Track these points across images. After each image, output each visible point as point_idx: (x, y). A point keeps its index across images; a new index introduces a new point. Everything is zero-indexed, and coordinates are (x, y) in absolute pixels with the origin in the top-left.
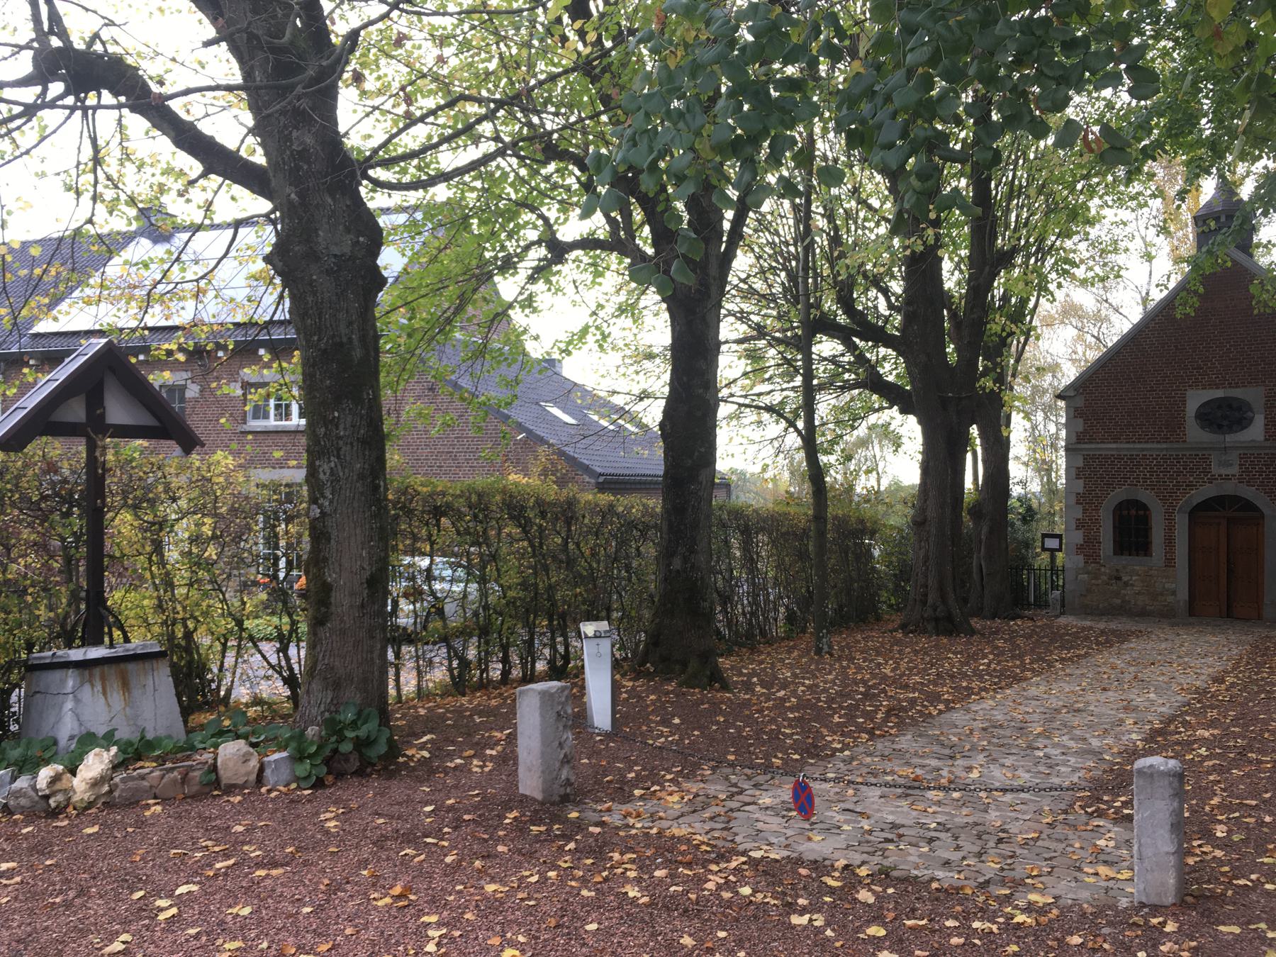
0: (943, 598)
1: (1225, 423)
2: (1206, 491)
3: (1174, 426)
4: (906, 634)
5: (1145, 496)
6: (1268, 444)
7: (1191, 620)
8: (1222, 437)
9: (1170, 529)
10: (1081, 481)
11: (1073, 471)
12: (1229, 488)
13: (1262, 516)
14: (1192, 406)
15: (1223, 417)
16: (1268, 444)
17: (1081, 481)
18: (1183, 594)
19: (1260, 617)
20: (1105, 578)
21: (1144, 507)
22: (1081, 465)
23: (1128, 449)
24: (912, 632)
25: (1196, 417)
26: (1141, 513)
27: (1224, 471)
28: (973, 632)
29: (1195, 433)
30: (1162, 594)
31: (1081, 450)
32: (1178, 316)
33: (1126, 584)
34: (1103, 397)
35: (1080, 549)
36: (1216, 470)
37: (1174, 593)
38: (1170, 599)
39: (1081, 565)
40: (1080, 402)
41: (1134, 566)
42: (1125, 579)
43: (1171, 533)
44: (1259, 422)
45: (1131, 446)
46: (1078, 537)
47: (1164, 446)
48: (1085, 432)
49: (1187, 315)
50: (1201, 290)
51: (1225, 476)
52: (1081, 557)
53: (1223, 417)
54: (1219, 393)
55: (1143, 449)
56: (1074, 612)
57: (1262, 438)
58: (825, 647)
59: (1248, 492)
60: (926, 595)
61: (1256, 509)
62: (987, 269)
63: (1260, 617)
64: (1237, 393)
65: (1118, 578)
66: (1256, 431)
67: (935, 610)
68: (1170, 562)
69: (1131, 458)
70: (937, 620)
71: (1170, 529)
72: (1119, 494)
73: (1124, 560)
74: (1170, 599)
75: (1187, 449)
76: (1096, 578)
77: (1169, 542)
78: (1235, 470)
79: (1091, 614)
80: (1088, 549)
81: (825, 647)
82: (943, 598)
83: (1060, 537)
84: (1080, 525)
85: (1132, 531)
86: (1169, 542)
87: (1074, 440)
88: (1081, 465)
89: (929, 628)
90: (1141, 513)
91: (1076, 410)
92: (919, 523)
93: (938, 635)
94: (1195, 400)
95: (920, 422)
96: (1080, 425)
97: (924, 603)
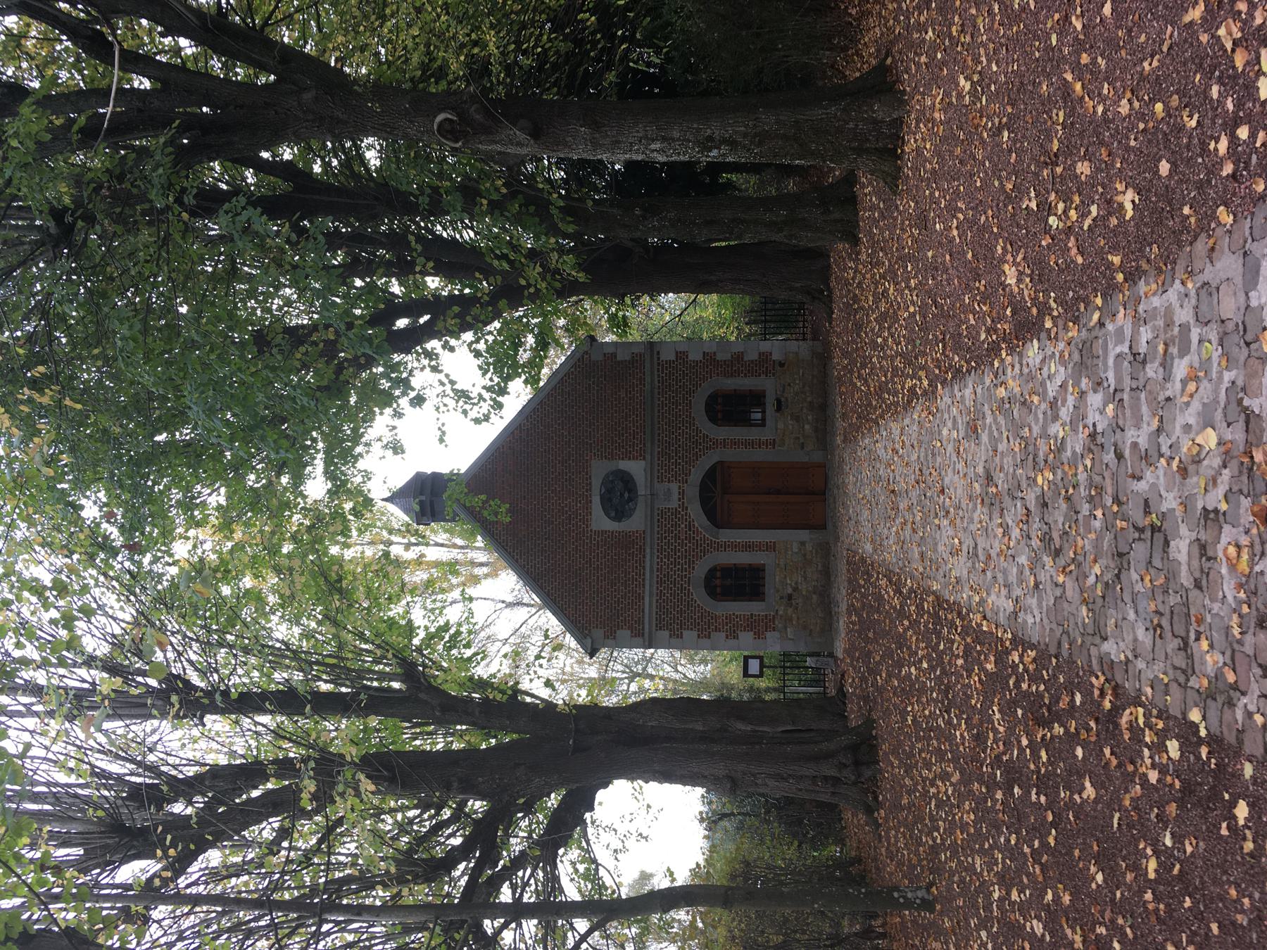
0: (827, 756)
1: (626, 495)
2: (695, 512)
3: (628, 542)
4: (879, 805)
5: (700, 570)
6: (648, 457)
7: (830, 526)
8: (641, 499)
9: (735, 547)
10: (685, 633)
11: (673, 641)
12: (693, 491)
13: (721, 463)
14: (608, 525)
15: (620, 495)
16: (648, 457)
17: (685, 633)
18: (804, 535)
19: (822, 466)
20: (790, 611)
21: (712, 571)
22: (667, 633)
23: (651, 586)
24: (876, 798)
25: (620, 521)
26: (718, 574)
27: (675, 496)
28: (869, 723)
29: (636, 522)
30: (804, 555)
31: (650, 633)
32: (508, 519)
33: (795, 589)
34: (595, 616)
35: (759, 635)
36: (674, 504)
37: (803, 543)
38: (809, 547)
39: (776, 634)
40: (598, 633)
41: (775, 582)
42: (790, 591)
43: (739, 546)
44: (625, 465)
45: (647, 582)
46: (746, 637)
47: (648, 551)
48: (631, 628)
49: (508, 511)
50: (483, 497)
51: (681, 495)
52: (768, 634)
53: (620, 495)
54: (596, 500)
55: (652, 571)
56: (831, 642)
57: (643, 463)
58: (920, 894)
59: (696, 476)
60: (826, 778)
61: (713, 470)
62: (422, 696)
63: (822, 466)
64: (596, 484)
65: (790, 597)
66: (636, 468)
67: (845, 766)
68: (771, 547)
69: (660, 582)
70: (857, 763)
71: (735, 547)
72: (699, 596)
73: (769, 590)
74: (809, 547)
75: (652, 529)
76: (791, 620)
77: (748, 547)
78: (674, 487)
79: (831, 625)
80: (758, 627)
81: (920, 894)
82: (827, 756)
83: (746, 659)
84: (733, 635)
85: (740, 583)
86: (748, 547)
87: (640, 640)
88: (667, 633)
89: (868, 773)
90: (720, 400)
91: (606, 637)
92: (732, 291)
93: (877, 762)
94: (601, 521)
95: (605, 785)
96: (624, 633)
97: (836, 781)
